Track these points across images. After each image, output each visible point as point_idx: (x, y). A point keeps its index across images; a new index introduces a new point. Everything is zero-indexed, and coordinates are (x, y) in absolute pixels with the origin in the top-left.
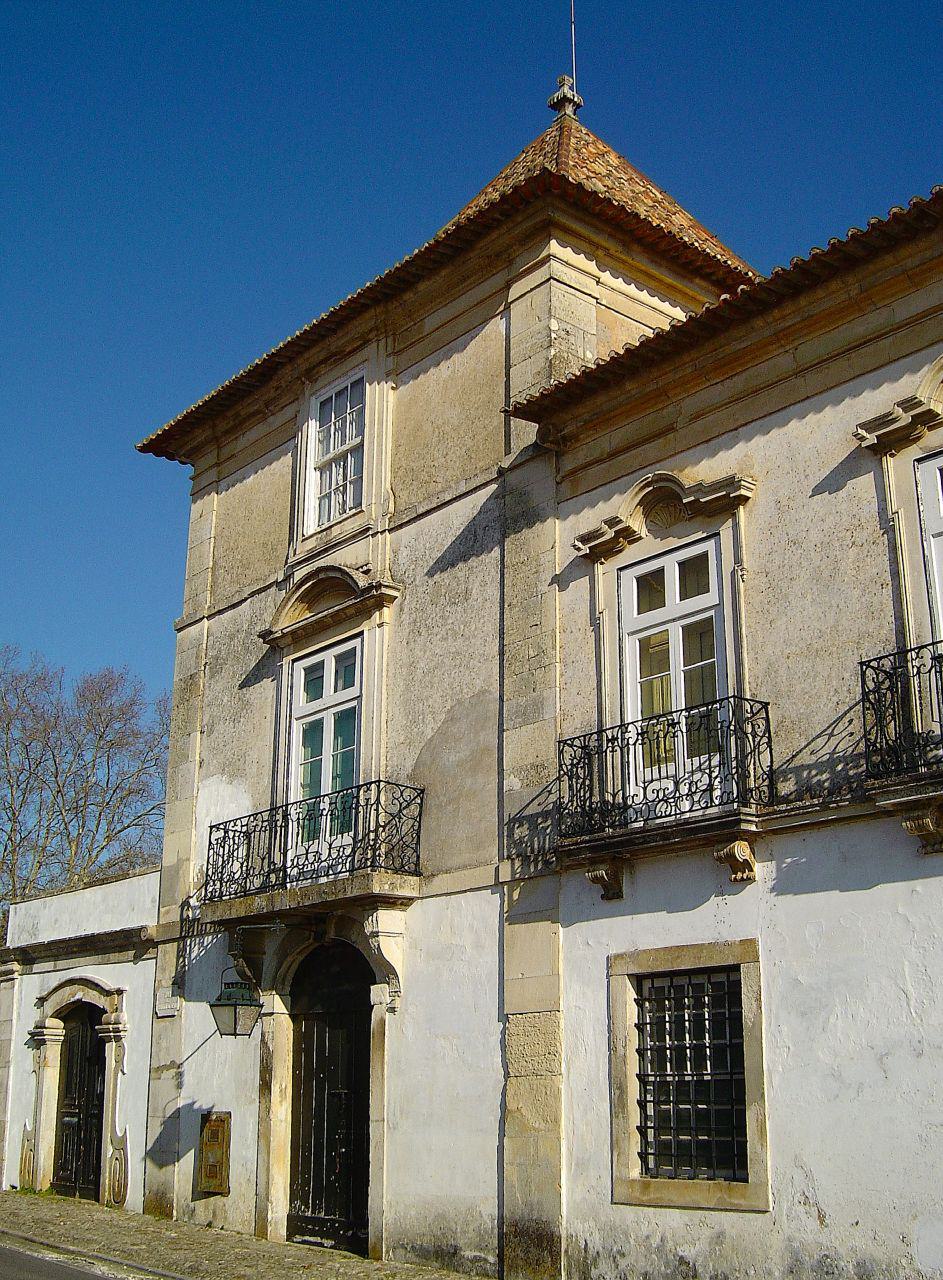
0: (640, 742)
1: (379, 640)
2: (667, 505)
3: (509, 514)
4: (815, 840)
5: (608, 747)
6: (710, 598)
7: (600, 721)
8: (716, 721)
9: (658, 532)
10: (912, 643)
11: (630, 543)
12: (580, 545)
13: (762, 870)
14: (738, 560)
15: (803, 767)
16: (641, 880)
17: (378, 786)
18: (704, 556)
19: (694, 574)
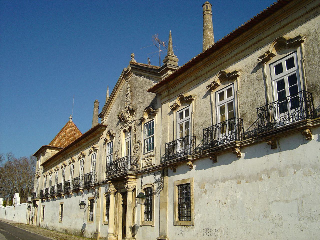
2: (282, 45)
4: (252, 148)
5: (269, 108)
6: (295, 68)
8: (232, 123)
9: (279, 53)
10: (269, 102)
11: (178, 107)
12: (260, 59)
13: (243, 155)
14: (302, 57)
15: (250, 132)
16: (283, 142)
18: (231, 88)
19: (230, 92)
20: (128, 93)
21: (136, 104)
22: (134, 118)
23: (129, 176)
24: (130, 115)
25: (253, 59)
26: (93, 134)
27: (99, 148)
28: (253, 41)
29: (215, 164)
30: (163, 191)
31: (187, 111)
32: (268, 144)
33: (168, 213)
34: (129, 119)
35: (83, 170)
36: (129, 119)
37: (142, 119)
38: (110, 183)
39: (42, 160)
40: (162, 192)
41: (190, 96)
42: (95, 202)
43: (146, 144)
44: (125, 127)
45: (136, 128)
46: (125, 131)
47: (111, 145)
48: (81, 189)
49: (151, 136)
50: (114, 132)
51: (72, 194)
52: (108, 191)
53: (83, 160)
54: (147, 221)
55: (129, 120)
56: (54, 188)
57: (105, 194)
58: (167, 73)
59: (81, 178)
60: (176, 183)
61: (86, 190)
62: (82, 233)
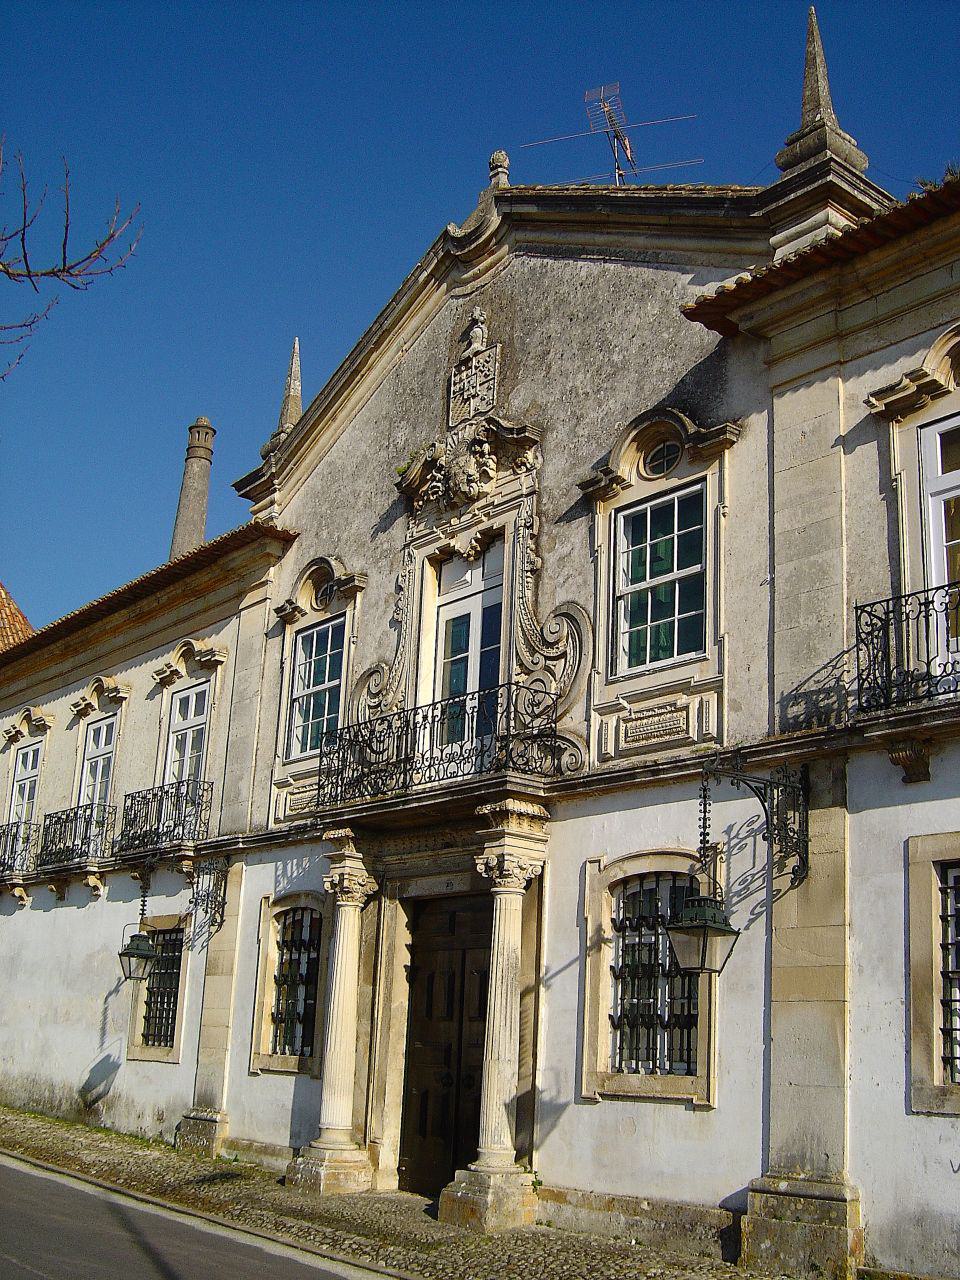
0: (923, 614)
3: (385, 524)
7: (896, 585)
11: (302, 616)
17: (509, 690)
20: (477, 354)
21: (543, 409)
22: (526, 482)
23: (512, 805)
24: (497, 464)
25: (845, 398)
26: (182, 596)
27: (228, 660)
30: (805, 899)
31: (201, 696)
32: (895, 762)
33: (847, 1030)
34: (487, 488)
35: (31, 797)
36: (487, 488)
37: (601, 480)
38: (340, 842)
40: (789, 907)
41: (211, 652)
42: (193, 946)
43: (298, 720)
44: (452, 535)
45: (544, 539)
46: (442, 559)
47: (327, 643)
48: (96, 869)
49: (328, 684)
50: (355, 565)
52: (327, 886)
53: (103, 725)
54: (283, 1053)
55: (481, 495)
57: (275, 903)
58: (820, 216)
60: (926, 852)
61: (52, 890)
62: (88, 1106)
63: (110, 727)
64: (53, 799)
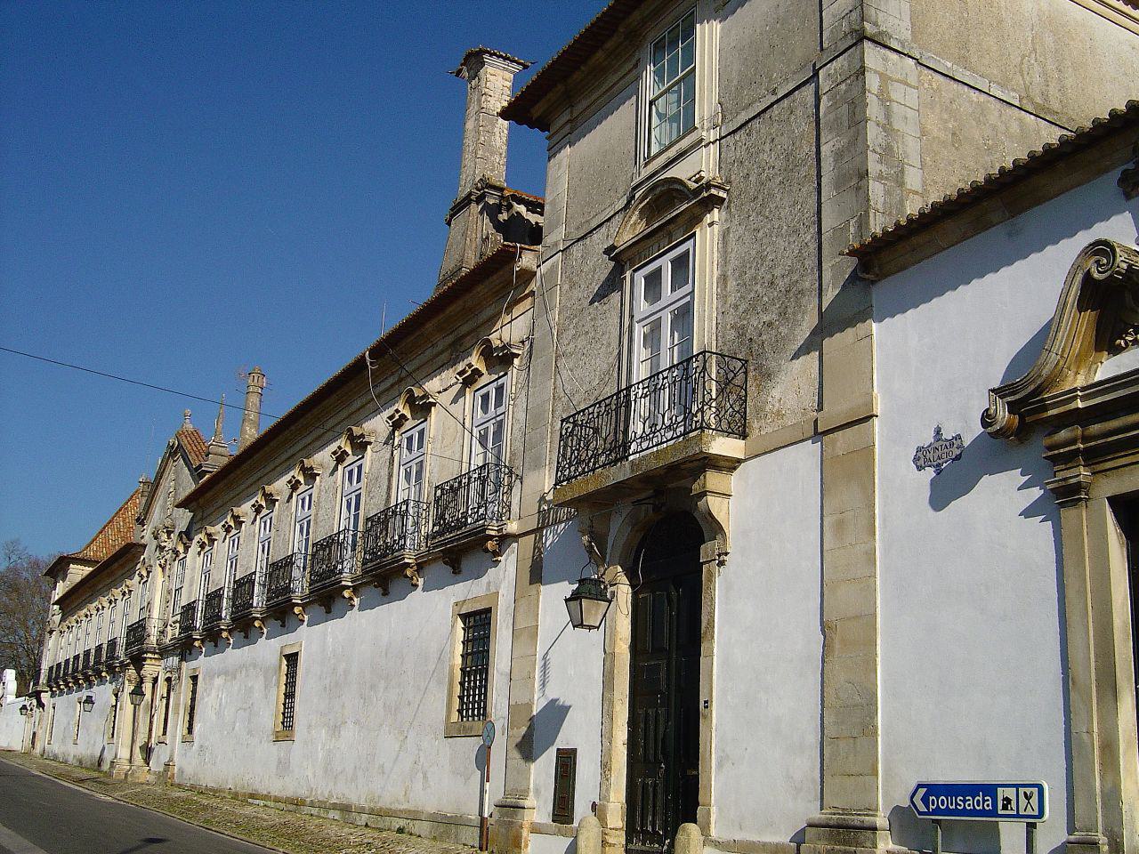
1: (707, 240)
28: (255, 477)
29: (385, 598)
39: (61, 589)
48: (350, 584)
51: (262, 626)
56: (221, 597)
59: (82, 656)
63: (421, 433)
64: (438, 471)
